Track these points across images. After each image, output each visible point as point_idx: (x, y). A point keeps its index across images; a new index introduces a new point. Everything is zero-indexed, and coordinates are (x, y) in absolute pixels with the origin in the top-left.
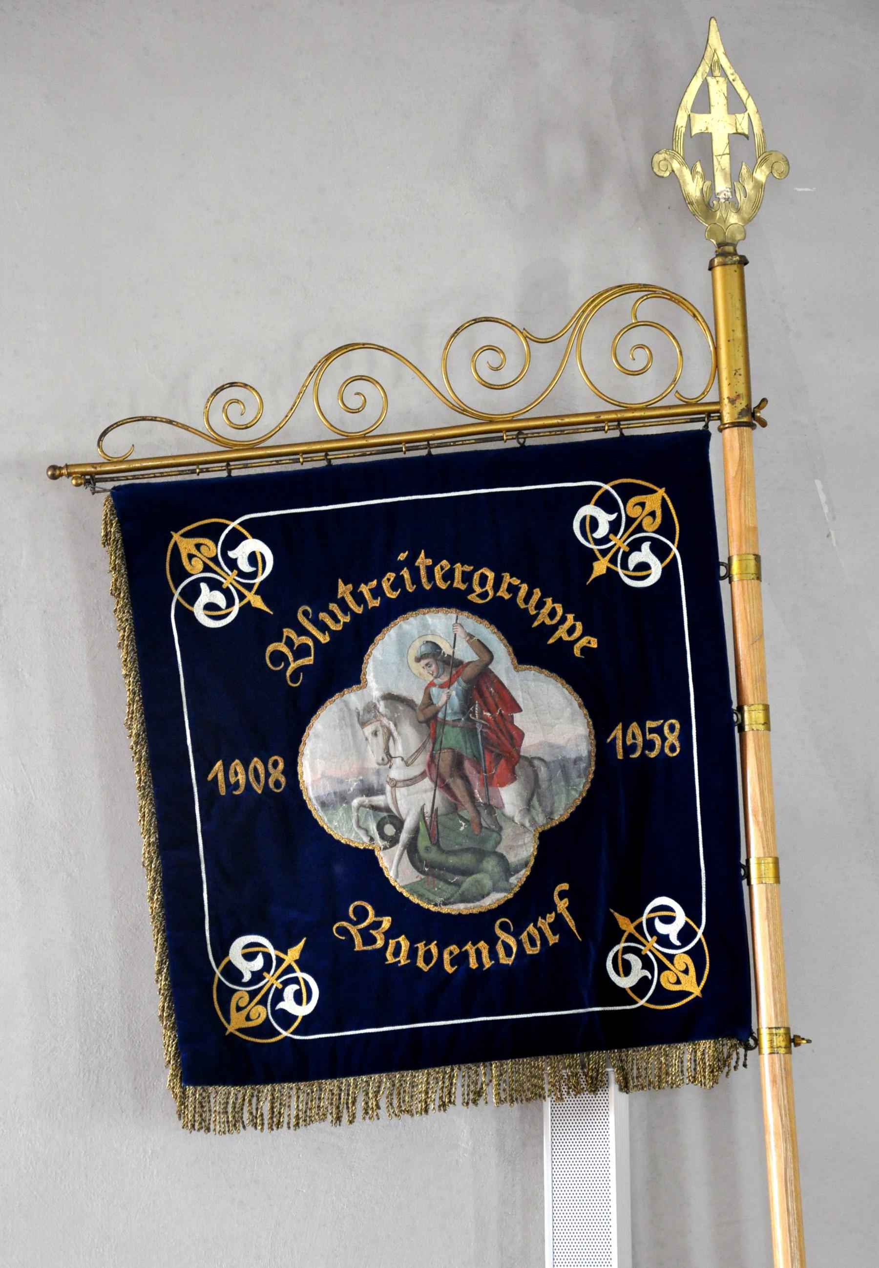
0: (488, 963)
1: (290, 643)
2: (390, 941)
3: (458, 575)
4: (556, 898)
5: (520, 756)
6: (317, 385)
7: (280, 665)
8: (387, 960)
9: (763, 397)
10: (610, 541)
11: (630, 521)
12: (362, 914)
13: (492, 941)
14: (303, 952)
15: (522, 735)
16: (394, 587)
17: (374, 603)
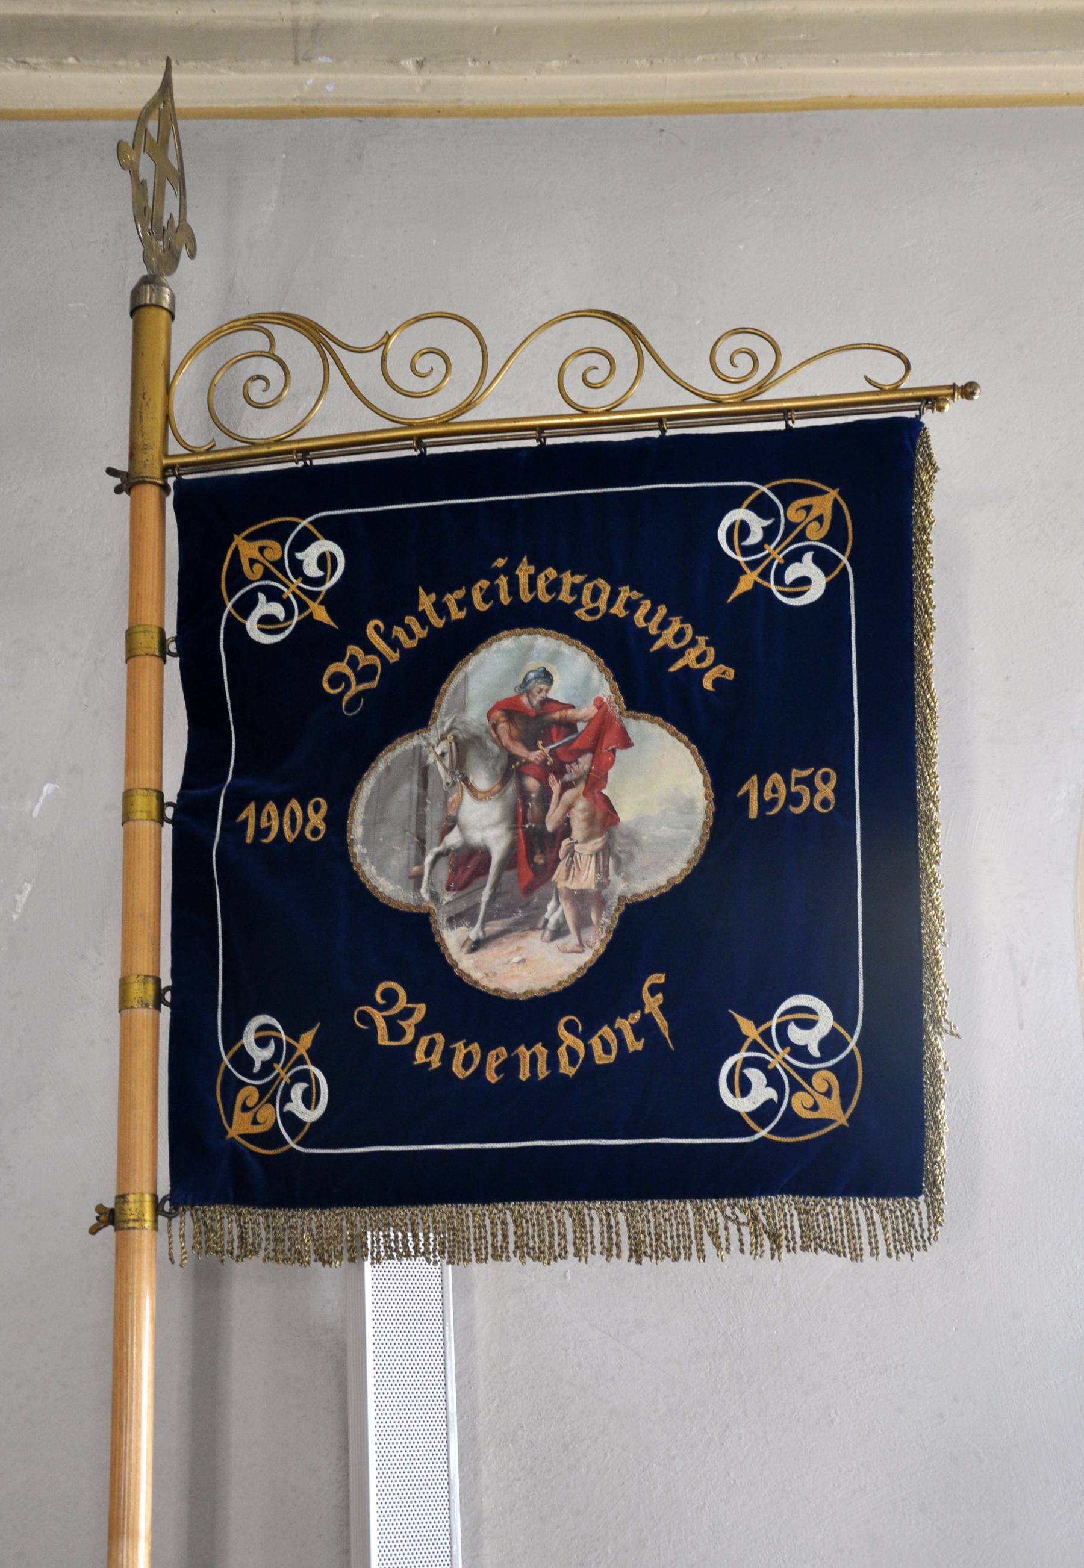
1: (353, 662)
3: (566, 588)
7: (340, 685)
8: (415, 1060)
9: (972, 379)
11: (790, 526)
12: (391, 997)
13: (553, 1044)
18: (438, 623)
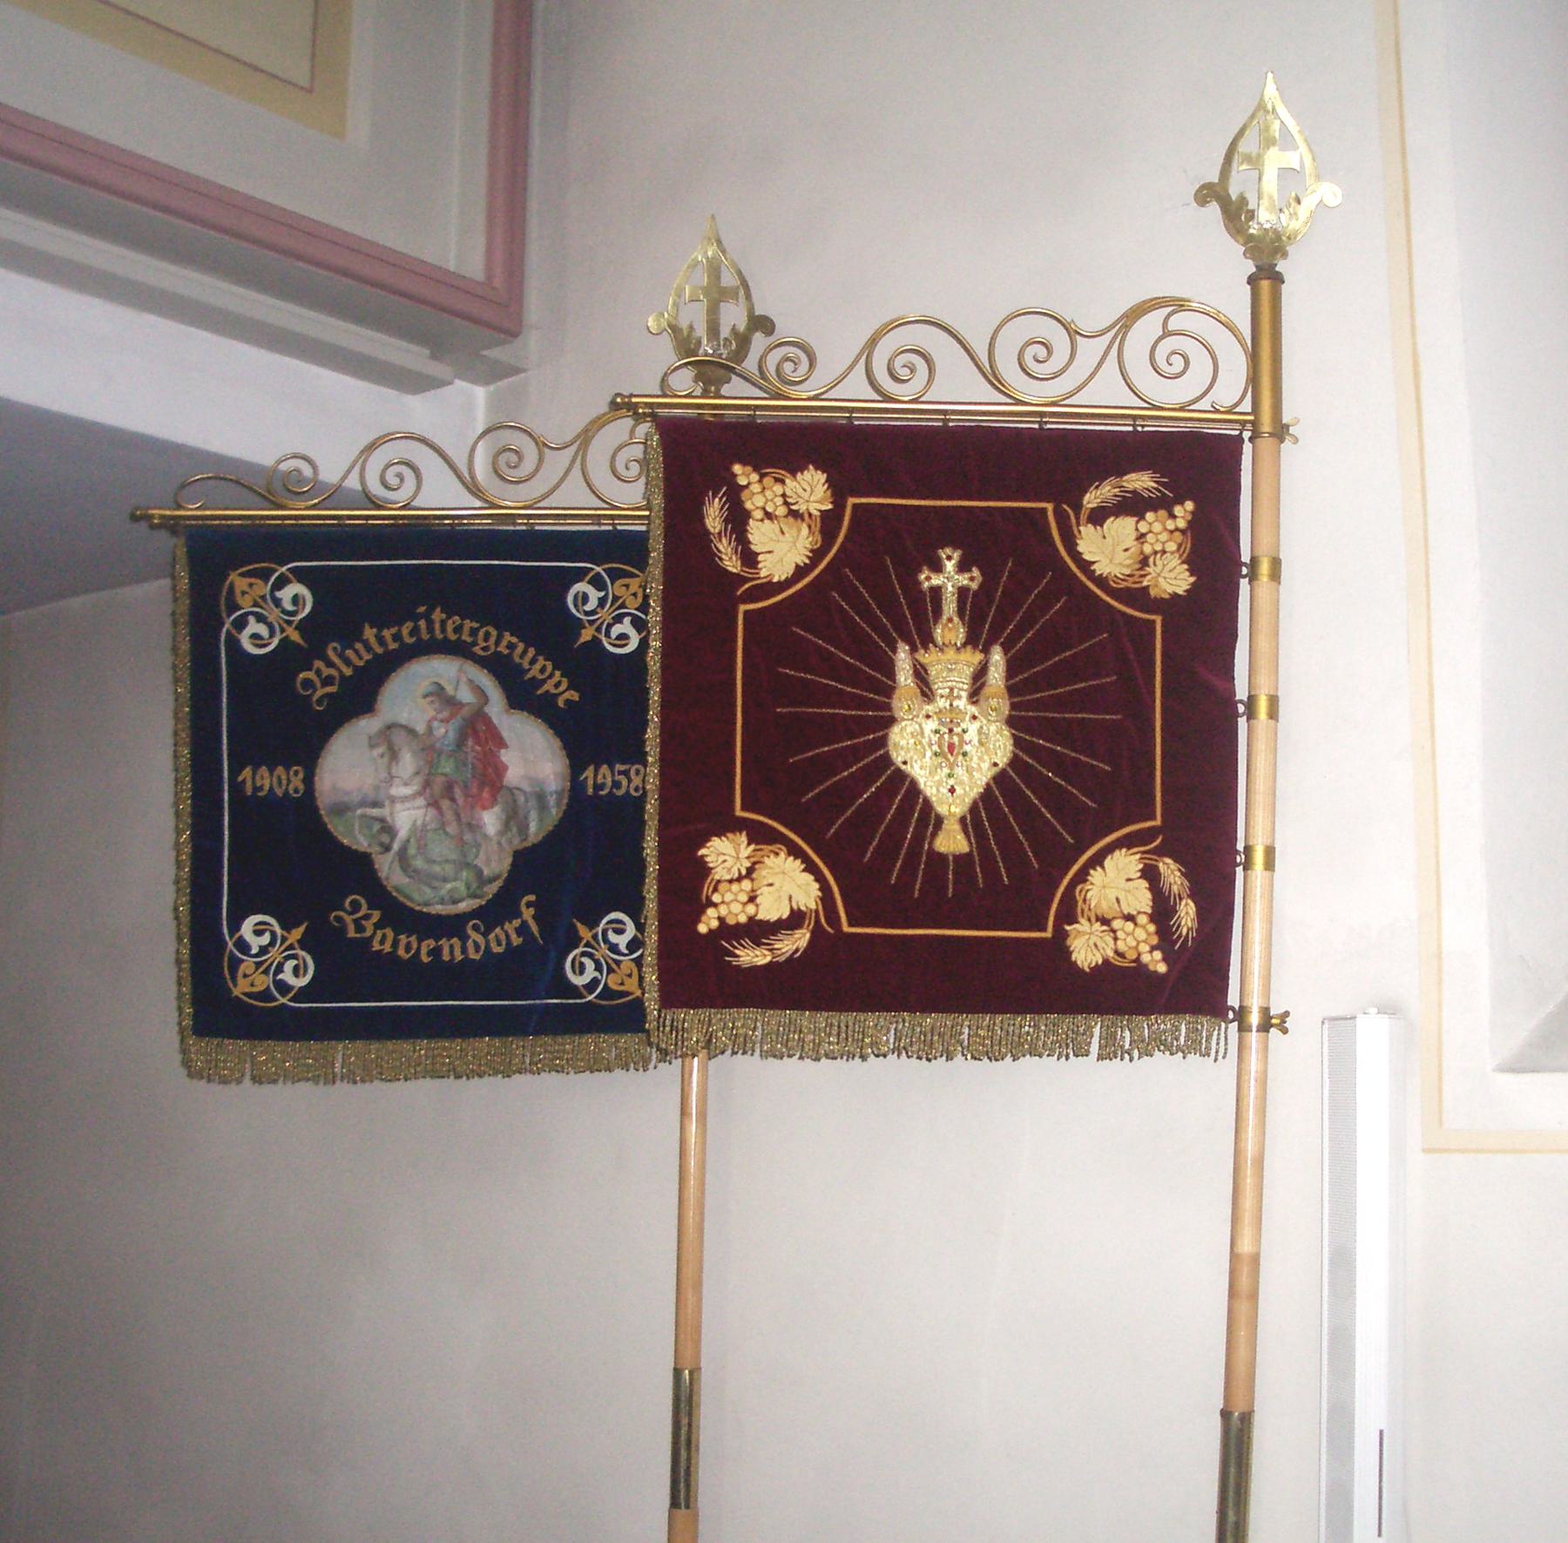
0: (459, 957)
1: (318, 672)
2: (378, 931)
3: (466, 629)
4: (523, 908)
5: (502, 787)
6: (365, 462)
7: (307, 691)
10: (597, 613)
12: (356, 907)
13: (464, 938)
14: (305, 934)
15: (505, 768)
16: (411, 634)
17: (393, 646)
18: (380, 650)
